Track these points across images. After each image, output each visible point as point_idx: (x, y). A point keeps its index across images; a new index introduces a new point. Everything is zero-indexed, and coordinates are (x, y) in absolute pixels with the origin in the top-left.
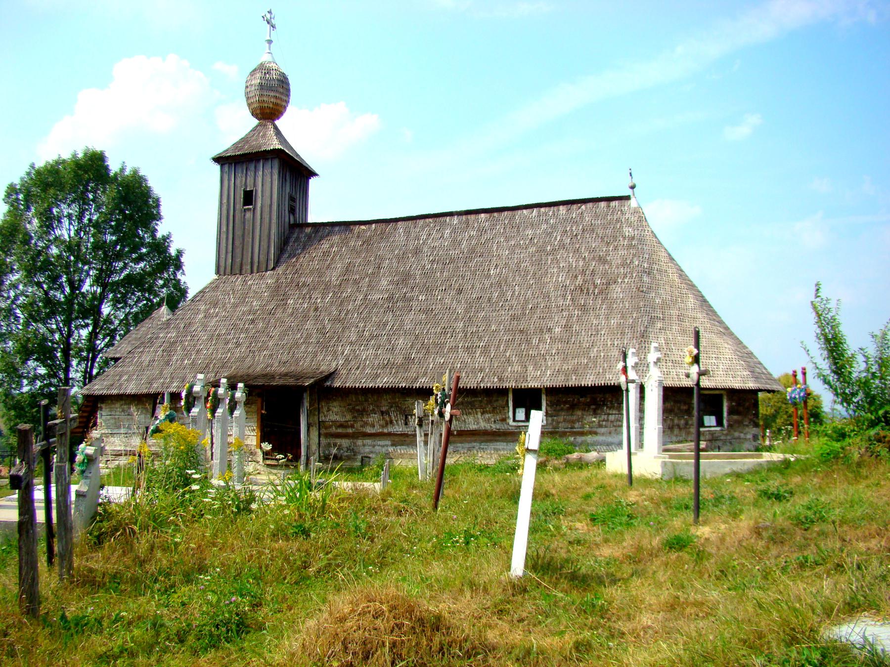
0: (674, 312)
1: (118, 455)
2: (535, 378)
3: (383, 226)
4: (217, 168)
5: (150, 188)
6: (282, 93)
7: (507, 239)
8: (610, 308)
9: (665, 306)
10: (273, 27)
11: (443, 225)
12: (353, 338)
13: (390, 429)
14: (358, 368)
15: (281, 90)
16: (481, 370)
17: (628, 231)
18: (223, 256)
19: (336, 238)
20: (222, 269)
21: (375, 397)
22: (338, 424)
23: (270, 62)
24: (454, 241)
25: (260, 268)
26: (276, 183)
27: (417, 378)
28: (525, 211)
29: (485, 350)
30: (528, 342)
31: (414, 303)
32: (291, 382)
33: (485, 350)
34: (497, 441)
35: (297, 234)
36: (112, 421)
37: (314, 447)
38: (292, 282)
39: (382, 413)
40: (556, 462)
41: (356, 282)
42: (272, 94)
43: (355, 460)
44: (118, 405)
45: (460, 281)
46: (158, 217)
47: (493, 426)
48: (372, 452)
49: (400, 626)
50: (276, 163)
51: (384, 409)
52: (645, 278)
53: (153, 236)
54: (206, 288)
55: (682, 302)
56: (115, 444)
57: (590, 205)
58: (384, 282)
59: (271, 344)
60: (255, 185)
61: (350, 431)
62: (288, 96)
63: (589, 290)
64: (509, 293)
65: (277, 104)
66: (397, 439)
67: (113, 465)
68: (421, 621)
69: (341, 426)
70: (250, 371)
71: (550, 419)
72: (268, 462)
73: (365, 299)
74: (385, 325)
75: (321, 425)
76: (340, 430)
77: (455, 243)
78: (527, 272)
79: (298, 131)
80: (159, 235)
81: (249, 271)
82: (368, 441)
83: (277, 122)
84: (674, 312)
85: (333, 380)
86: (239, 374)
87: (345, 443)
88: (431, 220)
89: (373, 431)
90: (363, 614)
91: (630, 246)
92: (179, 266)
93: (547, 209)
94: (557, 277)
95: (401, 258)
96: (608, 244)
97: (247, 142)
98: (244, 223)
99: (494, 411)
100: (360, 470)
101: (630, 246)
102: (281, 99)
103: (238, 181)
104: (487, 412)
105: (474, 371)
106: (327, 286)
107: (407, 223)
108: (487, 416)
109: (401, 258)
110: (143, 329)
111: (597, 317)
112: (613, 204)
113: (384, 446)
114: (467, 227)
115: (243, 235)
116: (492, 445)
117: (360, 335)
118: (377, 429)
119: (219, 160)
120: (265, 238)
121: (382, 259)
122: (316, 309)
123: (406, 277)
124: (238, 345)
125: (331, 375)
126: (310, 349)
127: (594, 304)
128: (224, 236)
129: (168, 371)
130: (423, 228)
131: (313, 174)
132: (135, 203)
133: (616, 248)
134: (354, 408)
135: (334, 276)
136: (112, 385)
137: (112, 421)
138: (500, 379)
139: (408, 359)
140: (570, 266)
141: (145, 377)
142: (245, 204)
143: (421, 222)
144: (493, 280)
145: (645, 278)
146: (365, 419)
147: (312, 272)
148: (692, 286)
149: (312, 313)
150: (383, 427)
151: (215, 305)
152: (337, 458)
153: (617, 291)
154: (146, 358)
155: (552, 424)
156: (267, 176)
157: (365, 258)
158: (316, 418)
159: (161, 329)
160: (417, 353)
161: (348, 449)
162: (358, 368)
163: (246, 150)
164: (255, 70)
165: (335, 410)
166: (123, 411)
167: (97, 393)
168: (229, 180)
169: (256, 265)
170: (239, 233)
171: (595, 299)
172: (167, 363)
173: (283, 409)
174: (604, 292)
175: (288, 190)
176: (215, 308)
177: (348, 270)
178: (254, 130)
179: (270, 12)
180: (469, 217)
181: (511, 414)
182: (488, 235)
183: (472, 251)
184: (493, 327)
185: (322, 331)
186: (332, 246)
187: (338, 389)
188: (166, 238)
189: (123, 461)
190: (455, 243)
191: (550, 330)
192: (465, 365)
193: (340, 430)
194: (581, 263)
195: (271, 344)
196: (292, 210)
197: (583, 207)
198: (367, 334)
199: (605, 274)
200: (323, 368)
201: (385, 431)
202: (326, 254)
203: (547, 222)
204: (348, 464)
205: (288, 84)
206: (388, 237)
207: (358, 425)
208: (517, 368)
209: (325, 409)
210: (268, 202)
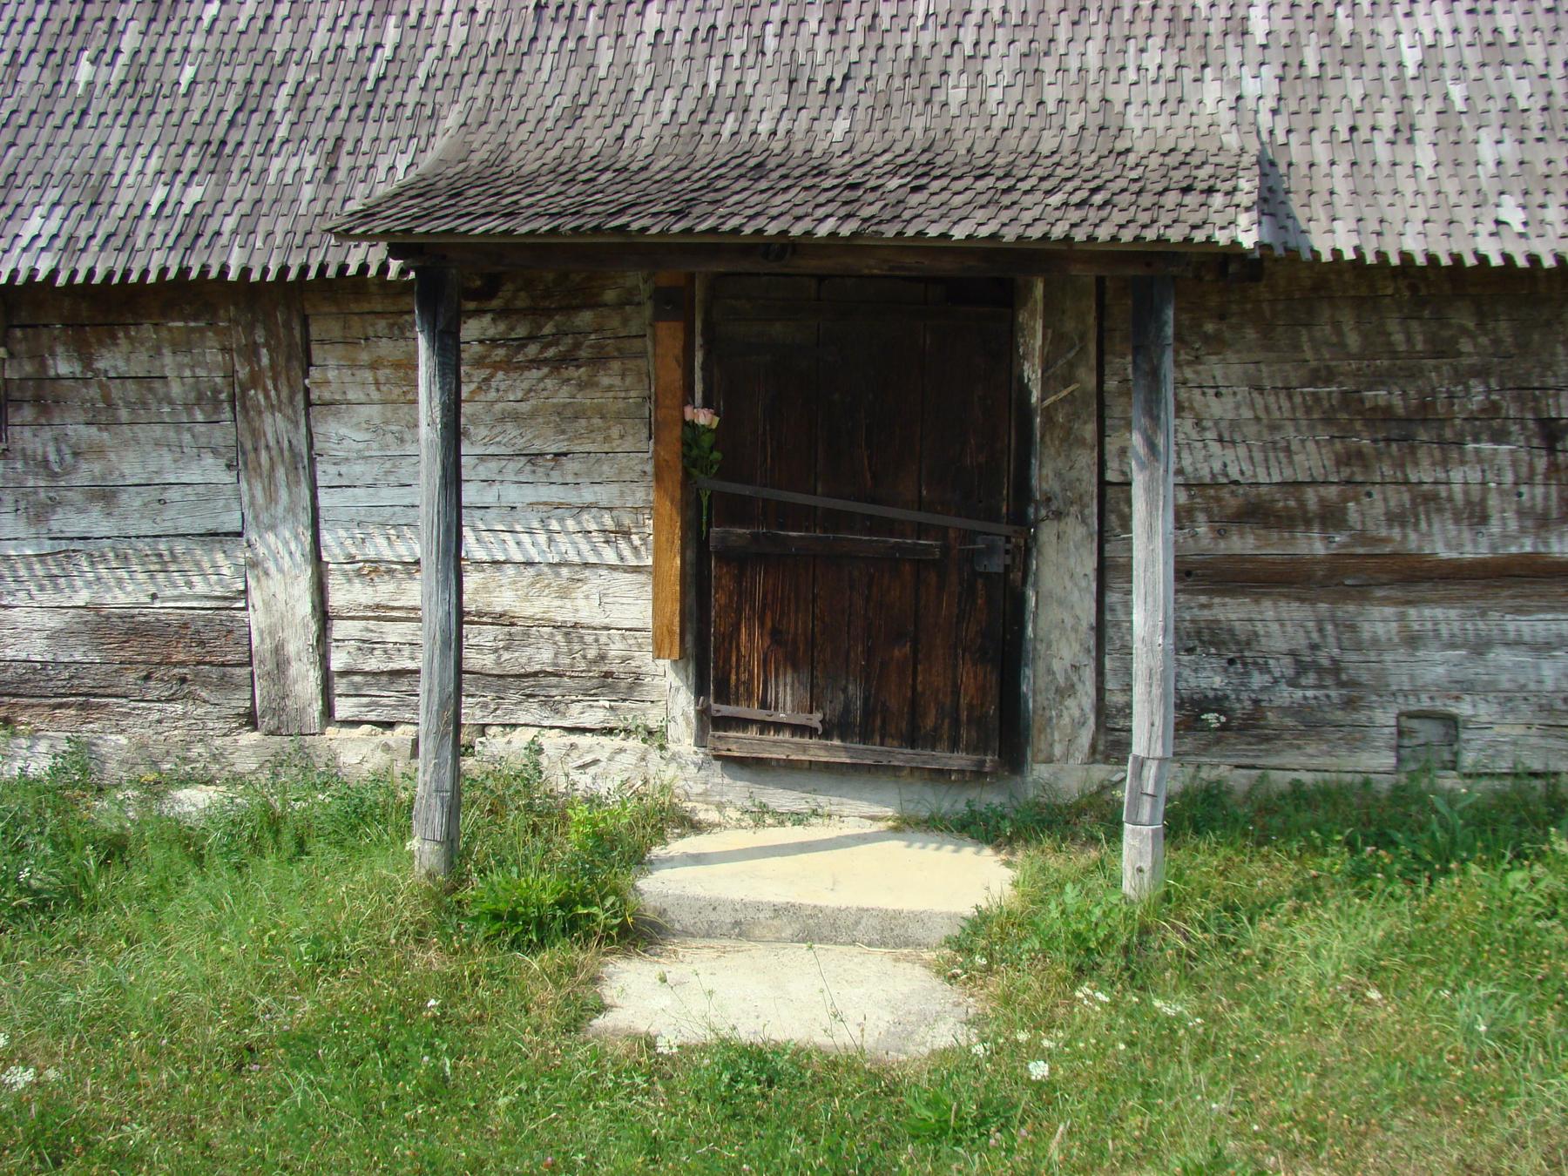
21: (1504, 328)
22: (1232, 503)
48: (1466, 688)
56: (85, 314)
61: (1313, 545)
72: (741, 743)
76: (1243, 543)
82: (1442, 617)
89: (1474, 548)
118: (1504, 536)
134: (1349, 401)
146: (1424, 473)
158: (1085, 460)
161: (1301, 668)
165: (1217, 408)
180: (319, 483)
193: (1243, 543)
207: (1369, 513)
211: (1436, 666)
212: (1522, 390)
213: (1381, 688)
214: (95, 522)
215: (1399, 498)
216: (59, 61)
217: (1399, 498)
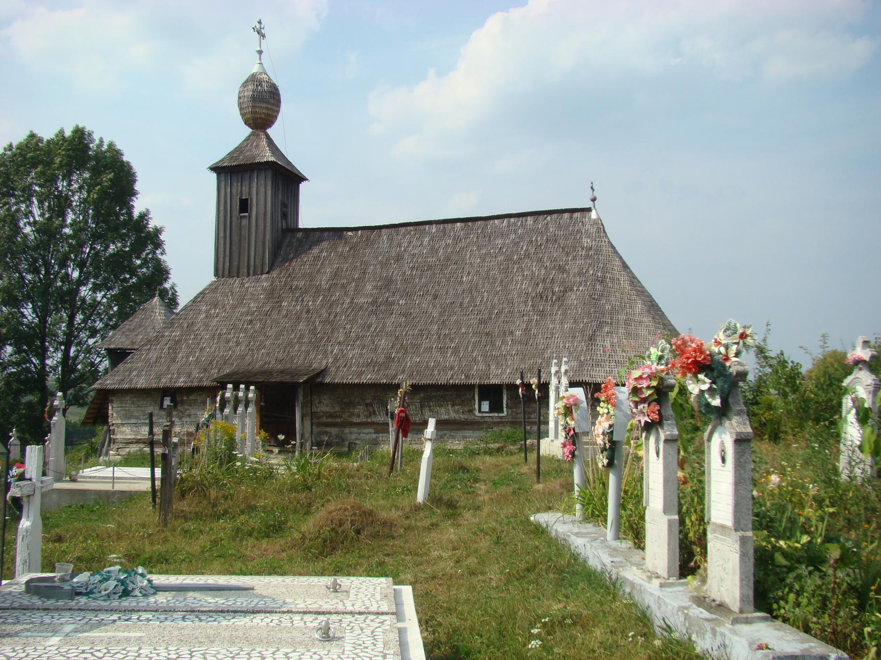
0: (622, 317)
1: (129, 442)
2: (496, 376)
3: (369, 232)
4: (214, 175)
5: (128, 163)
6: (273, 104)
7: (479, 248)
8: (564, 314)
9: (613, 312)
10: (263, 36)
11: (423, 234)
12: (341, 338)
13: (374, 419)
14: (345, 366)
15: (273, 101)
16: (451, 368)
17: (586, 242)
18: (221, 260)
19: (325, 244)
20: (220, 272)
23: (261, 73)
24: (432, 248)
25: (258, 271)
26: (269, 192)
27: (396, 375)
28: (496, 221)
29: (456, 351)
30: (493, 343)
31: (395, 307)
32: (287, 378)
33: (456, 351)
34: (465, 429)
35: (291, 241)
36: (123, 413)
37: (307, 435)
38: (285, 285)
39: (367, 405)
40: (512, 447)
41: (344, 286)
42: (264, 105)
43: (343, 446)
44: (128, 398)
45: (437, 288)
46: (133, 193)
47: (462, 417)
48: (357, 439)
49: (355, 514)
50: (269, 174)
51: (368, 401)
52: (598, 287)
53: (130, 213)
54: (205, 289)
55: (631, 307)
57: (555, 216)
58: (369, 287)
59: (268, 343)
60: (250, 194)
62: (279, 106)
63: (548, 297)
64: (479, 299)
65: (269, 115)
66: (379, 428)
67: (124, 452)
68: (364, 512)
69: (331, 416)
70: (250, 368)
71: (510, 411)
73: (352, 302)
74: (369, 327)
75: (313, 415)
76: (330, 420)
77: (433, 251)
78: (495, 279)
79: (290, 137)
80: (136, 213)
81: (246, 274)
82: (355, 430)
83: (269, 131)
84: (622, 317)
85: (324, 376)
86: (241, 371)
87: (334, 431)
88: (412, 228)
89: (358, 421)
90: (340, 509)
91: (587, 256)
92: (158, 244)
93: (516, 219)
94: (521, 284)
95: (385, 264)
96: (568, 254)
97: (241, 152)
98: (241, 229)
99: (462, 404)
100: (348, 454)
101: (587, 256)
102: (272, 110)
103: (234, 190)
104: (456, 404)
105: (445, 370)
106: (318, 290)
107: (389, 230)
108: (456, 408)
109: (385, 264)
110: (136, 320)
111: (553, 322)
112: (576, 215)
113: (368, 434)
114: (444, 235)
115: (240, 241)
116: (461, 434)
117: (348, 335)
119: (215, 169)
120: (260, 244)
121: (367, 264)
122: (308, 311)
123: (388, 282)
124: (238, 343)
125: (323, 372)
126: (303, 349)
127: (551, 310)
128: (222, 241)
129: (174, 367)
130: (404, 236)
131: (303, 179)
132: (115, 179)
133: (574, 258)
135: (323, 281)
136: (123, 380)
137: (123, 413)
138: (467, 377)
139: (389, 358)
140: (533, 274)
141: (153, 373)
142: (241, 211)
143: (403, 230)
144: (464, 286)
145: (598, 287)
146: (351, 410)
147: (304, 276)
148: (642, 292)
149: (304, 315)
150: (367, 417)
151: (216, 306)
152: (329, 445)
153: (572, 298)
154: (153, 355)
155: (511, 415)
156: (258, 187)
157: (352, 263)
158: (309, 409)
159: (165, 328)
160: (397, 352)
162: (345, 366)
163: (241, 160)
164: (247, 81)
165: (326, 402)
166: (133, 403)
167: (109, 387)
168: (225, 189)
169: (252, 269)
170: (235, 238)
171: (552, 305)
172: (174, 360)
173: (282, 402)
174: (561, 298)
175: (280, 197)
176: (215, 309)
177: (336, 274)
178: (247, 139)
179: (260, 22)
180: (446, 225)
181: (477, 406)
182: (463, 244)
183: (448, 258)
184: (463, 330)
185: (313, 332)
186: (322, 251)
187: (328, 384)
188: (144, 216)
189: (134, 448)
190: (433, 251)
191: (511, 333)
192: (438, 364)
193: (330, 420)
194: (543, 272)
195: (268, 343)
196: (284, 215)
197: (549, 218)
198: (353, 335)
199: (563, 282)
200: (314, 366)
201: (369, 420)
202: (317, 258)
203: (515, 232)
204: (338, 449)
205: (279, 95)
206: (372, 244)
207: (345, 416)
208: (482, 367)
209: (317, 402)
210: (262, 211)
213: (347, 440)
214: (188, 419)
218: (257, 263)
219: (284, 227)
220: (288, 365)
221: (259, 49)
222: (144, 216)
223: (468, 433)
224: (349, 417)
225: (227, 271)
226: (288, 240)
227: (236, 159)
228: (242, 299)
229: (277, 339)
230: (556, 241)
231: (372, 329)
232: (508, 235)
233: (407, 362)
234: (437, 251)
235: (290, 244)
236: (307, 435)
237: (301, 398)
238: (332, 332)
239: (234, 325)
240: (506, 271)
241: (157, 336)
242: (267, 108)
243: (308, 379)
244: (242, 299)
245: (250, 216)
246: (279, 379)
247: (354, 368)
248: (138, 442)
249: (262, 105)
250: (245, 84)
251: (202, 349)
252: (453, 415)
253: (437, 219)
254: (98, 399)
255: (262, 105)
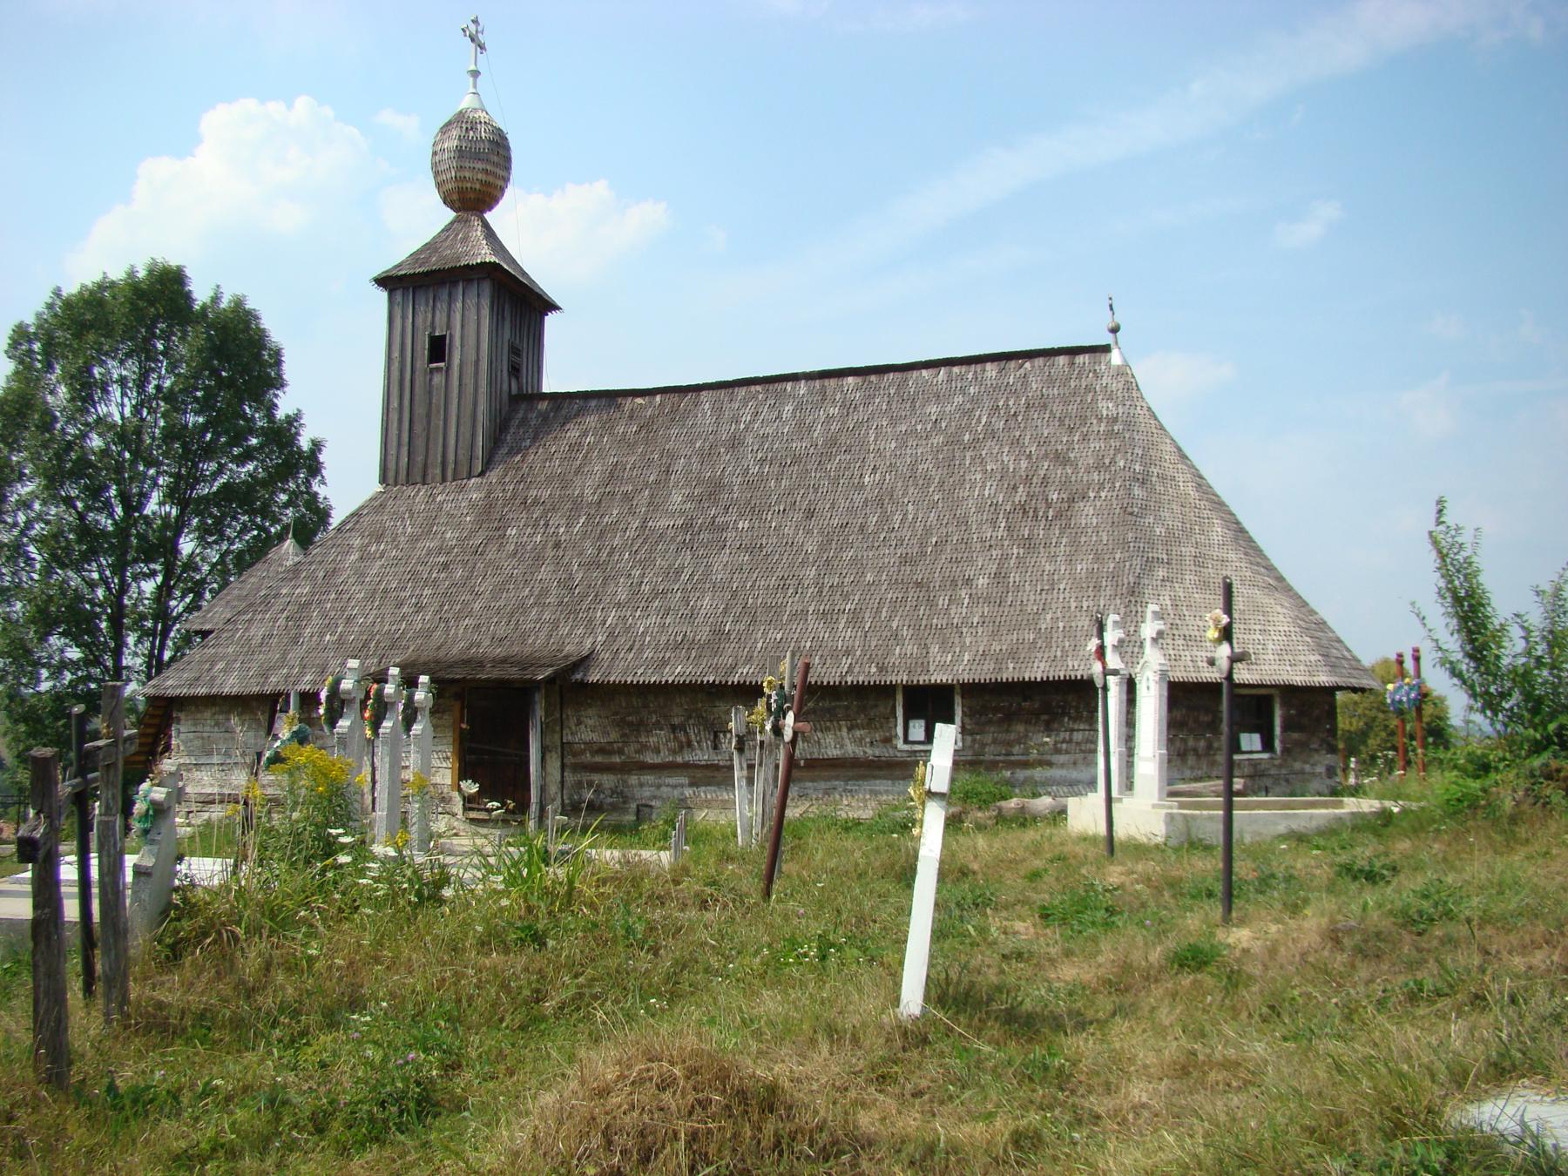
0: (1188, 550)
1: (208, 801)
2: (942, 666)
3: (675, 398)
4: (383, 295)
5: (264, 331)
6: (497, 165)
7: (893, 422)
8: (1074, 543)
9: (1171, 539)
10: (482, 47)
11: (781, 397)
12: (622, 596)
14: (630, 649)
15: (495, 159)
16: (848, 653)
17: (1106, 407)
18: (393, 451)
19: (591, 420)
20: (391, 474)
23: (475, 110)
24: (800, 424)
25: (458, 473)
27: (734, 667)
28: (924, 373)
29: (855, 618)
30: (931, 603)
31: (731, 535)
32: (513, 673)
33: (855, 618)
34: (875, 778)
35: (523, 412)
36: (198, 743)
37: (553, 789)
38: (514, 497)
39: (674, 728)
40: (980, 814)
42: (479, 166)
43: (625, 811)
44: (207, 714)
46: (278, 383)
47: (869, 751)
50: (487, 288)
51: (676, 721)
52: (1137, 491)
53: (270, 416)
54: (362, 508)
57: (1039, 361)
58: (677, 497)
59: (477, 606)
60: (449, 327)
61: (617, 759)
62: (508, 168)
63: (1038, 511)
64: (897, 517)
65: (488, 184)
66: (699, 774)
69: (602, 751)
70: (441, 654)
71: (969, 738)
72: (473, 815)
73: (643, 526)
74: (678, 573)
75: (565, 748)
76: (598, 759)
77: (803, 429)
78: (928, 480)
80: (280, 415)
81: (439, 478)
82: (649, 778)
83: (488, 216)
84: (1188, 550)
85: (587, 669)
86: (422, 660)
87: (608, 780)
88: (759, 388)
89: (657, 760)
90: (640, 1081)
91: (1110, 434)
92: (315, 469)
93: (964, 369)
94: (980, 488)
95: (708, 455)
96: (1071, 430)
97: (436, 250)
98: (430, 393)
99: (870, 724)
100: (634, 829)
101: (1110, 434)
103: (419, 320)
104: (858, 727)
105: (835, 655)
106: (577, 505)
107: (716, 393)
108: (858, 733)
109: (708, 455)
110: (252, 580)
111: (1053, 558)
112: (1080, 359)
113: (676, 787)
114: (823, 400)
115: (428, 416)
116: (867, 785)
117: (635, 590)
118: (665, 757)
119: (385, 281)
120: (466, 420)
121: (673, 456)
122: (557, 545)
123: (715, 489)
124: (419, 608)
125: (584, 662)
126: (546, 616)
127: (1046, 536)
128: (394, 416)
129: (295, 655)
130: (745, 402)
131: (552, 307)
132: (237, 356)
133: (1085, 438)
135: (588, 488)
136: (197, 679)
137: (198, 743)
138: (881, 669)
139: (719, 633)
140: (1004, 469)
141: (255, 665)
142: (432, 359)
145: (1137, 491)
147: (549, 480)
148: (1219, 505)
149: (550, 553)
150: (674, 752)
151: (379, 538)
152: (593, 808)
153: (1087, 514)
154: (257, 632)
155: (971, 747)
156: (468, 311)
157: (643, 454)
158: (557, 737)
162: (630, 649)
163: (434, 263)
164: (449, 123)
165: (591, 722)
166: (217, 724)
167: (170, 693)
168: (404, 318)
169: (451, 467)
170: (420, 410)
171: (1048, 527)
172: (295, 641)
174: (1064, 515)
176: (379, 543)
177: (612, 476)
178: (447, 229)
179: (475, 22)
180: (826, 382)
181: (900, 730)
182: (861, 415)
183: (832, 442)
184: (869, 577)
185: (567, 584)
186: (585, 434)
188: (293, 420)
190: (803, 429)
191: (968, 582)
192: (819, 644)
193: (598, 759)
194: (1024, 464)
195: (477, 606)
196: (515, 370)
197: (1028, 365)
198: (646, 588)
199: (1065, 483)
200: (568, 649)
201: (679, 759)
202: (575, 447)
203: (963, 391)
204: (614, 818)
205: (508, 149)
207: (630, 749)
208: (911, 648)
209: (573, 721)
211: (647, 792)
212: (665, 717)
213: (633, 798)
215: (637, 746)
216: (322, 635)
217: (637, 746)
218: (461, 457)
219: (514, 390)
220: (516, 649)
221: (473, 67)
222: (293, 420)
223: (881, 785)
224: (638, 752)
225: (403, 473)
226: (520, 415)
227: (427, 260)
228: (431, 522)
229: (495, 598)
230: (1045, 406)
231: (684, 577)
232: (950, 396)
233: (756, 641)
234: (810, 429)
235: (524, 421)
236: (553, 789)
237: (539, 712)
238: (604, 584)
239: (414, 573)
240: (949, 464)
241: (266, 596)
242: (486, 171)
243: (556, 672)
244: (431, 522)
245: (448, 368)
246: (495, 674)
247: (648, 654)
248: (223, 800)
249: (476, 172)
250: (445, 129)
251: (349, 620)
252: (851, 749)
253: (808, 370)
254: (153, 716)
255: (476, 172)
